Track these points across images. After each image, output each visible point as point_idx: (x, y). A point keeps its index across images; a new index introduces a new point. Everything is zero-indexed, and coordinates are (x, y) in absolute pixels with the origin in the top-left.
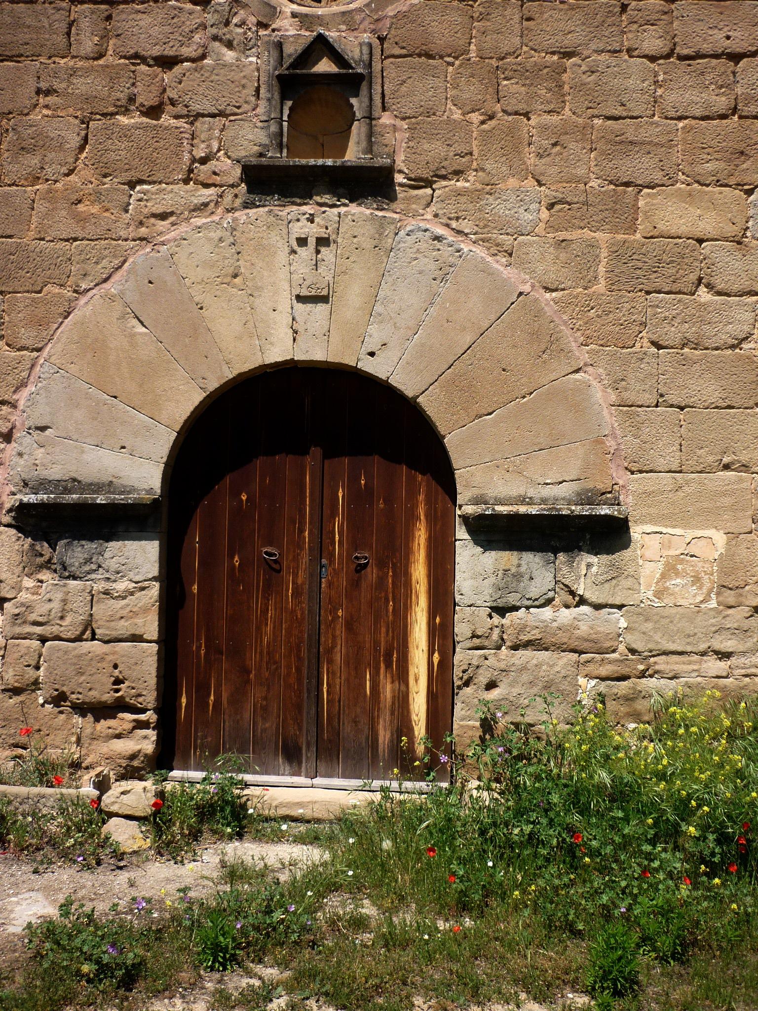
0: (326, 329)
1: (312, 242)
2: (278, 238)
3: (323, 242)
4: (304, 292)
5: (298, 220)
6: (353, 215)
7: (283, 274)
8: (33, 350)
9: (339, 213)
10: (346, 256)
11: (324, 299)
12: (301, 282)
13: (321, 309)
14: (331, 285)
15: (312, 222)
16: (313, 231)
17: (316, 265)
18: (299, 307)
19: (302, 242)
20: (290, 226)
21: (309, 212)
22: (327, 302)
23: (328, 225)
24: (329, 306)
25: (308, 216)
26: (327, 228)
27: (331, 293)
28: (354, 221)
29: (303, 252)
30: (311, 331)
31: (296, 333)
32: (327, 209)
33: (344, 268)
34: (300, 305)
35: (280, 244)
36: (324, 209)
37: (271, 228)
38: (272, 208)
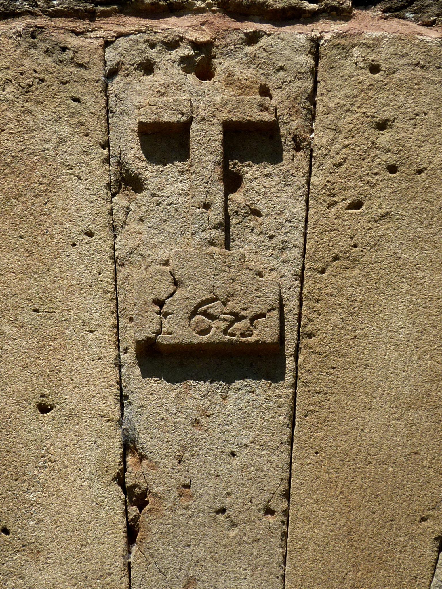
0: (273, 483)
1: (206, 142)
2: (65, 130)
3: (251, 141)
4: (178, 331)
5: (147, 67)
6: (373, 46)
7: (85, 265)
8: (353, 98)
9: (315, 42)
10: (351, 197)
11: (261, 361)
12: (162, 290)
13: (249, 401)
14: (292, 305)
15: (205, 73)
16: (210, 104)
17: (225, 225)
18: (155, 394)
19: (166, 141)
20: (115, 86)
21: (192, 35)
22: (275, 374)
23: (272, 83)
24: (282, 389)
25: (185, 51)
26: (265, 91)
27: (291, 336)
28: (375, 69)
29: (166, 181)
30: (208, 493)
31: (141, 501)
32: (266, 27)
33: (345, 242)
34: (157, 385)
35: (71, 154)
36: (250, 27)
37: (36, 93)
38: (40, 21)
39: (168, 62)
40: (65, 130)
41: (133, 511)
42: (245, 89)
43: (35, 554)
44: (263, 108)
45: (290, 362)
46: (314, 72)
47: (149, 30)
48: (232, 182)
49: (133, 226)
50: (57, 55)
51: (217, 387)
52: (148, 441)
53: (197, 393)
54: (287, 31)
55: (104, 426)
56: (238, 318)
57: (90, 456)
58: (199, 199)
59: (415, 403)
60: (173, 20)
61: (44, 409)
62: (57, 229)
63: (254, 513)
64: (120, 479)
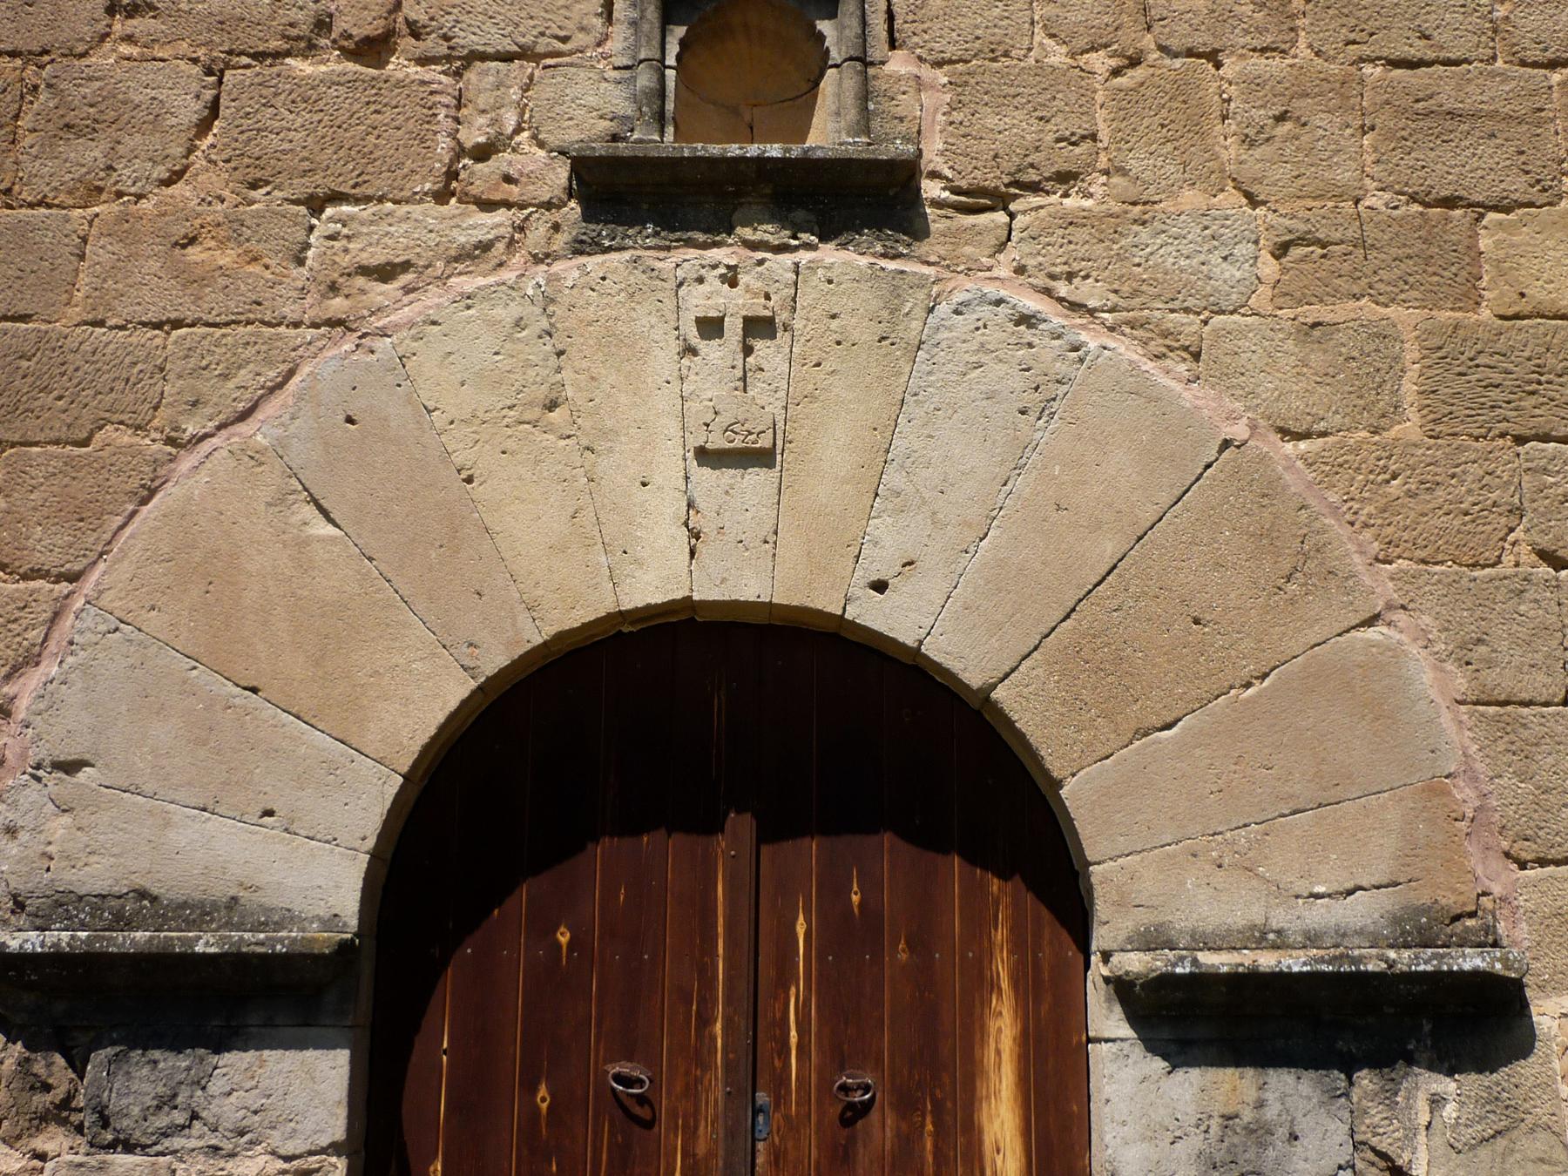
0: (768, 527)
1: (733, 327)
2: (654, 320)
3: (759, 327)
4: (717, 442)
5: (700, 280)
6: (829, 268)
7: (666, 400)
9: (797, 265)
10: (815, 360)
11: (763, 458)
12: (709, 417)
13: (757, 478)
14: (780, 425)
16: (736, 304)
19: (711, 327)
23: (771, 290)
25: (723, 270)
26: (767, 297)
27: (779, 443)
28: (830, 282)
29: (711, 350)
33: (811, 387)
34: (706, 471)
35: (657, 334)
36: (760, 255)
37: (637, 297)
38: (640, 253)
39: (712, 276)
40: (654, 320)
41: (693, 541)
42: (756, 295)
43: (641, 565)
44: (765, 307)
45: (779, 457)
46: (796, 284)
47: (702, 257)
48: (748, 351)
49: (692, 377)
50: (649, 274)
51: (739, 472)
52: (700, 503)
53: (728, 475)
54: (781, 257)
55: (678, 494)
56: (751, 433)
57: (670, 511)
58: (729, 363)
59: (845, 481)
60: (715, 250)
61: (644, 484)
62: (649, 380)
63: (758, 543)
64: (686, 524)
